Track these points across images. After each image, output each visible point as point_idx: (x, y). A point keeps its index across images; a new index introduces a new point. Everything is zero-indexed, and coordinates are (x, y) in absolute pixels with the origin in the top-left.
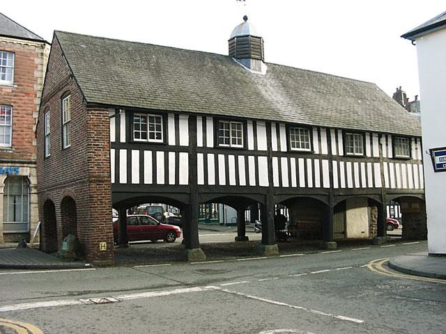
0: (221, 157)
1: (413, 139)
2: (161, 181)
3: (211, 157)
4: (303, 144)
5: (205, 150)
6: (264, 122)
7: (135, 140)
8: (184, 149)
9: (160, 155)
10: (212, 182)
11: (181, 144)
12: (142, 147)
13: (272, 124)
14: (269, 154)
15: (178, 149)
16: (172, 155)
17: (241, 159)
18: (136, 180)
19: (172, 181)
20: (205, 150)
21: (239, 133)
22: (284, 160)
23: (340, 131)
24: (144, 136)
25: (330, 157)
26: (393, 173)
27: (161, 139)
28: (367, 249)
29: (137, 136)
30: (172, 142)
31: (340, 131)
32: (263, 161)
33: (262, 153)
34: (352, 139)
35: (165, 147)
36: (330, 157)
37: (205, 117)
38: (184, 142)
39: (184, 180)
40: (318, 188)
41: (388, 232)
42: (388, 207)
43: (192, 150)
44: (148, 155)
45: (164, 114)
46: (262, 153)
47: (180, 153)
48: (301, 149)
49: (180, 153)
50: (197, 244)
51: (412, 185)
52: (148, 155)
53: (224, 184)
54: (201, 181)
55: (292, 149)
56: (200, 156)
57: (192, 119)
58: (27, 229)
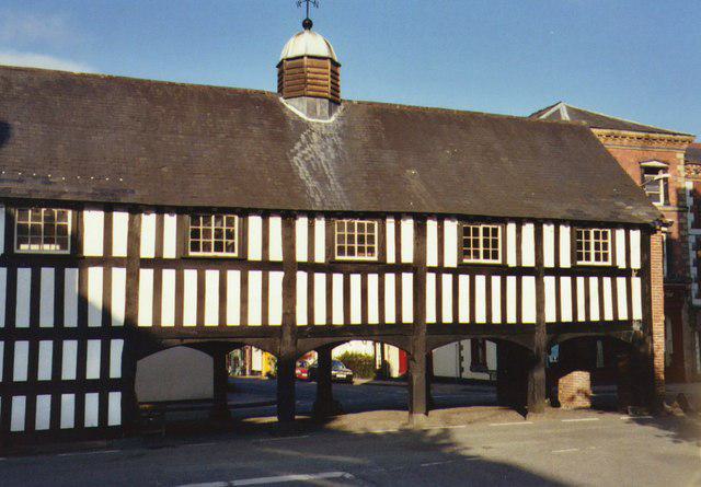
0: (190, 276)
3: (320, 278)
7: (192, 254)
8: (276, 266)
9: (373, 279)
12: (202, 264)
14: (289, 266)
17: (234, 277)
20: (158, 263)
21: (605, 246)
22: (566, 281)
24: (477, 255)
25: (289, 266)
26: (611, 308)
29: (195, 247)
30: (255, 254)
33: (529, 271)
36: (538, 272)
39: (408, 318)
40: (373, 326)
42: (615, 388)
45: (232, 211)
46: (529, 271)
47: (524, 278)
48: (213, 254)
49: (524, 278)
53: (467, 321)
55: (338, 258)
56: (302, 277)
57: (420, 221)
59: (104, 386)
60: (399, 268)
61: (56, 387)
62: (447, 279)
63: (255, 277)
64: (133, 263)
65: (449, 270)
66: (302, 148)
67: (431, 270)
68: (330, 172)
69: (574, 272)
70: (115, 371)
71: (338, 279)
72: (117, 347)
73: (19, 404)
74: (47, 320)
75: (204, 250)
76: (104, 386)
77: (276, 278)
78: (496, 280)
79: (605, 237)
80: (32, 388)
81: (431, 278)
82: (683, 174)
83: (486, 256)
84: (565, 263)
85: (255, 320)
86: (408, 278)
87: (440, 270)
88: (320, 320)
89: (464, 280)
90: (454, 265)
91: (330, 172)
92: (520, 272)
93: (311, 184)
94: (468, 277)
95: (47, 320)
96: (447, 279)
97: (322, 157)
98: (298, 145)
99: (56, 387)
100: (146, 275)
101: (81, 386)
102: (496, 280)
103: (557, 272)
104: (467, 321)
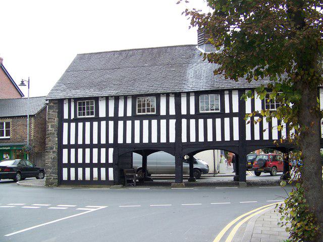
0: (137, 123)
6: (237, 91)
15: (231, 115)
17: (154, 122)
18: (146, 140)
21: (92, 108)
23: (72, 100)
28: (164, 189)
31: (72, 100)
37: (126, 98)
38: (172, 112)
39: (236, 137)
41: (202, 175)
43: (178, 117)
50: (244, 180)
54: (184, 140)
55: (78, 117)
56: (184, 121)
64: (116, 119)
71: (201, 121)
77: (173, 122)
85: (163, 140)
100: (121, 123)
101: (99, 165)
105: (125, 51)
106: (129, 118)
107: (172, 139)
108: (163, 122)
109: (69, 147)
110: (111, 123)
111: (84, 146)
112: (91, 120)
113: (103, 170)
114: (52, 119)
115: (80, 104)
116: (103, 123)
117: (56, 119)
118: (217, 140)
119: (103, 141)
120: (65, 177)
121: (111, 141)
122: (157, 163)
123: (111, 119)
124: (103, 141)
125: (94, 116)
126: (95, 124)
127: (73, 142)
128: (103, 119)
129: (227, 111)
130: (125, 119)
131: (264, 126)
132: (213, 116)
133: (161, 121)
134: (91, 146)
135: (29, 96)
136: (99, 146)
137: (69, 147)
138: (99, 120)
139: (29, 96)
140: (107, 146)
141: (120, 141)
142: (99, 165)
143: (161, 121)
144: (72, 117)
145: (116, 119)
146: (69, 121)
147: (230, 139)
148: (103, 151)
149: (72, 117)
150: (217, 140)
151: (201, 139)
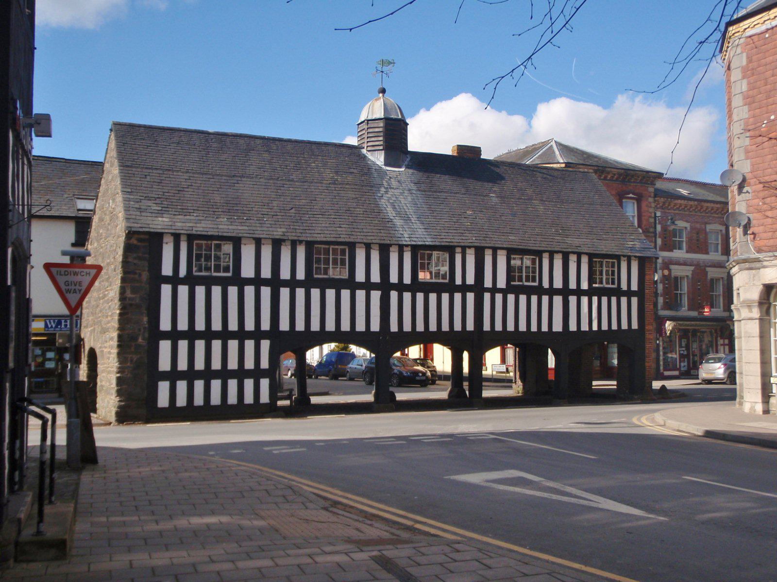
0: (315, 293)
1: (458, 250)
2: (534, 328)
3: (407, 296)
4: (607, 279)
5: (579, 293)
7: (316, 276)
10: (523, 327)
11: (554, 287)
12: (323, 285)
13: (165, 240)
16: (545, 299)
19: (545, 328)
27: (446, 279)
32: (558, 300)
33: (558, 292)
34: (601, 266)
35: (352, 285)
39: (470, 327)
42: (615, 383)
44: (331, 294)
46: (558, 292)
51: (726, 349)
52: (523, 298)
53: (333, 329)
54: (487, 327)
55: (195, 274)
56: (394, 295)
58: (665, 369)
59: (257, 374)
60: (464, 289)
61: (208, 375)
62: (499, 297)
63: (361, 294)
64: (275, 283)
65: (500, 291)
66: (386, 192)
67: (488, 290)
68: (410, 211)
69: (590, 293)
70: (265, 364)
71: (420, 296)
72: (265, 345)
73: (164, 387)
74: (200, 326)
75: (518, 281)
76: (257, 374)
77: (376, 295)
78: (534, 298)
79: (613, 266)
80: (173, 376)
81: (487, 296)
82: (653, 205)
83: (607, 283)
84: (585, 286)
85: (360, 327)
86: (470, 297)
87: (494, 290)
88: (458, 327)
89: (511, 298)
90: (504, 287)
91: (410, 211)
92: (552, 292)
93: (398, 222)
94: (364, 291)
95: (217, 326)
96: (499, 297)
97: (401, 198)
98: (383, 189)
99: (208, 375)
100: (285, 292)
101: (241, 374)
102: (445, 297)
103: (579, 293)
104: (333, 329)
105: (280, 140)
106: (300, 284)
107: (375, 327)
108: (361, 294)
109: (174, 335)
110: (266, 292)
111: (225, 335)
112: (225, 284)
113: (249, 384)
114: (135, 273)
115: (199, 247)
116: (249, 291)
117: (145, 275)
118: (253, 342)
119: (250, 326)
120: (163, 401)
121: (266, 326)
122: (27, 425)
123: (266, 282)
124: (250, 326)
125: (230, 274)
126: (233, 291)
127: (183, 325)
128: (249, 281)
129: (458, 281)
130: (293, 284)
131: (66, 263)
132: (439, 289)
133: (357, 291)
134: (191, 335)
135: (724, 347)
136: (241, 335)
137: (174, 335)
138: (241, 283)
139: (724, 347)
140: (257, 335)
141: (284, 326)
142: (241, 374)
143: (357, 291)
144: (183, 272)
145: (275, 283)
146: (175, 281)
147: (351, 328)
148: (249, 345)
149: (183, 272)
150: (253, 342)
151: (407, 328)
